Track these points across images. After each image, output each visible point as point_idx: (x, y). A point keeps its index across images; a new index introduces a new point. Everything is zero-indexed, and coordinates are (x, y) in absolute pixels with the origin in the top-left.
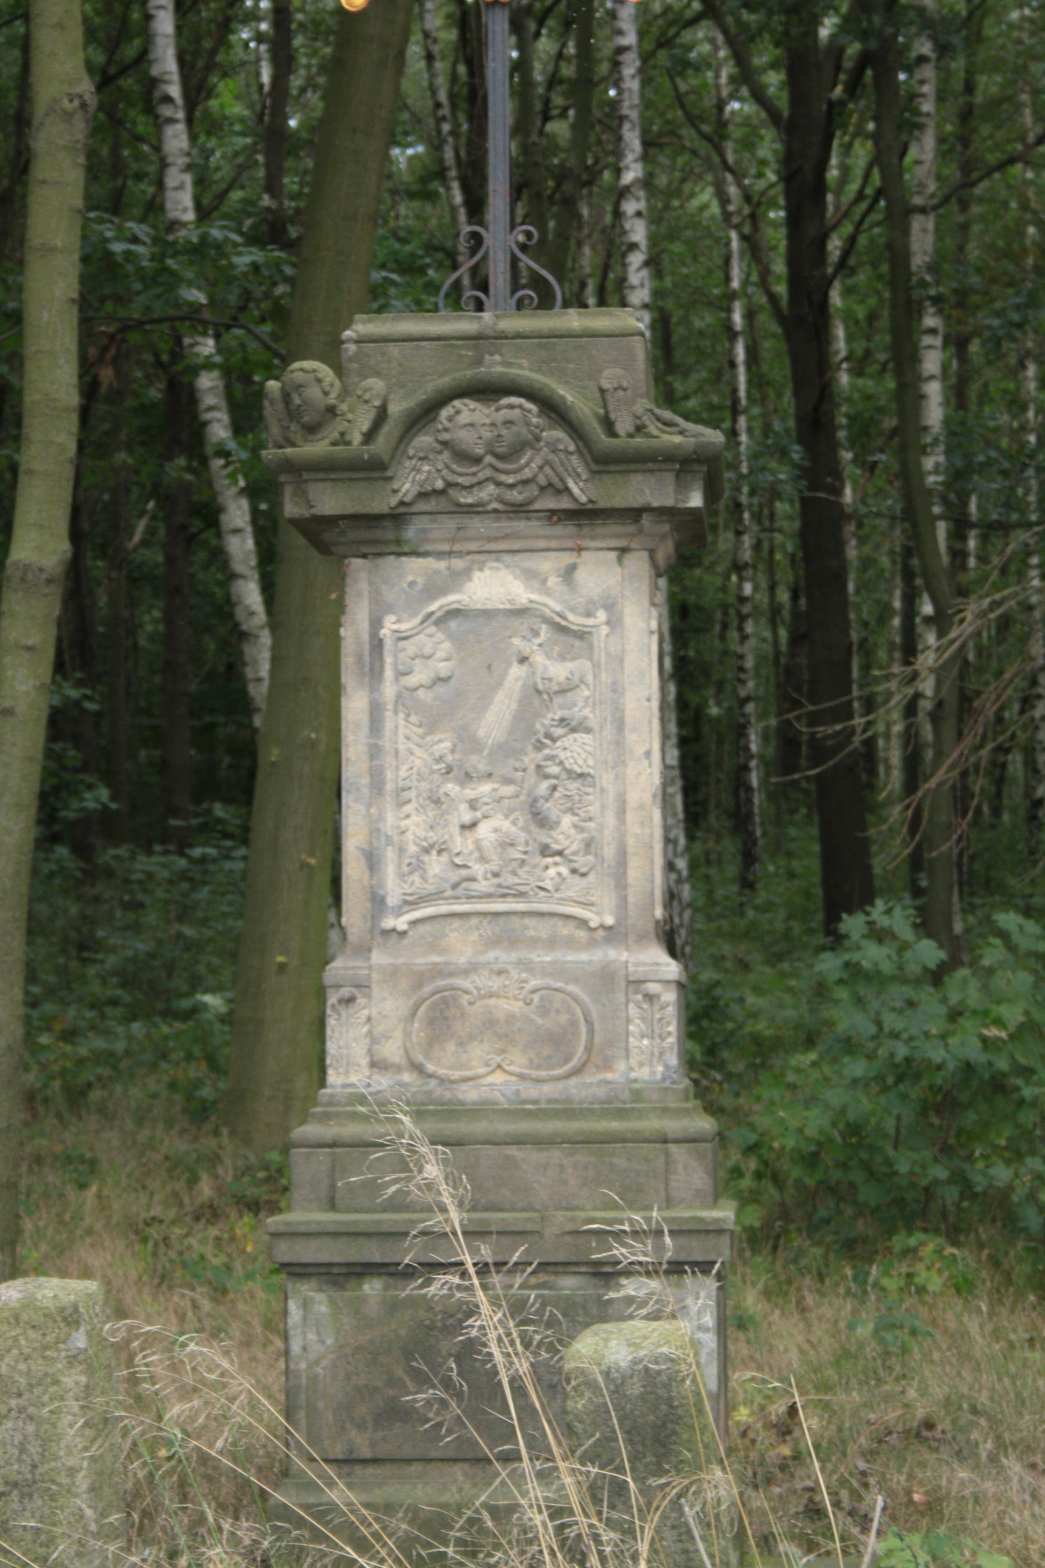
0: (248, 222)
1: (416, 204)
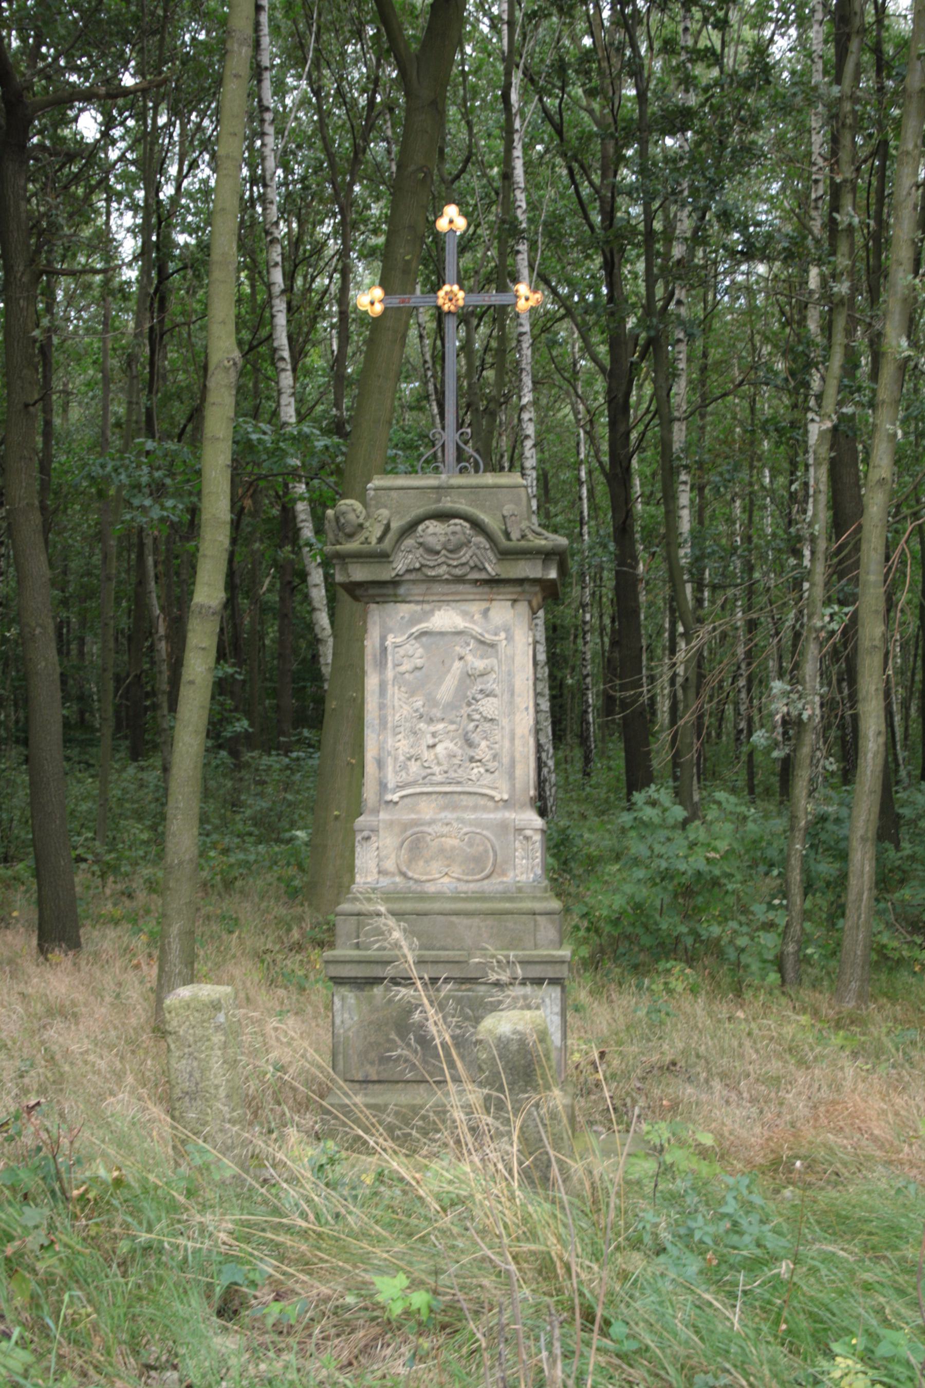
0: (324, 424)
1: (415, 413)
